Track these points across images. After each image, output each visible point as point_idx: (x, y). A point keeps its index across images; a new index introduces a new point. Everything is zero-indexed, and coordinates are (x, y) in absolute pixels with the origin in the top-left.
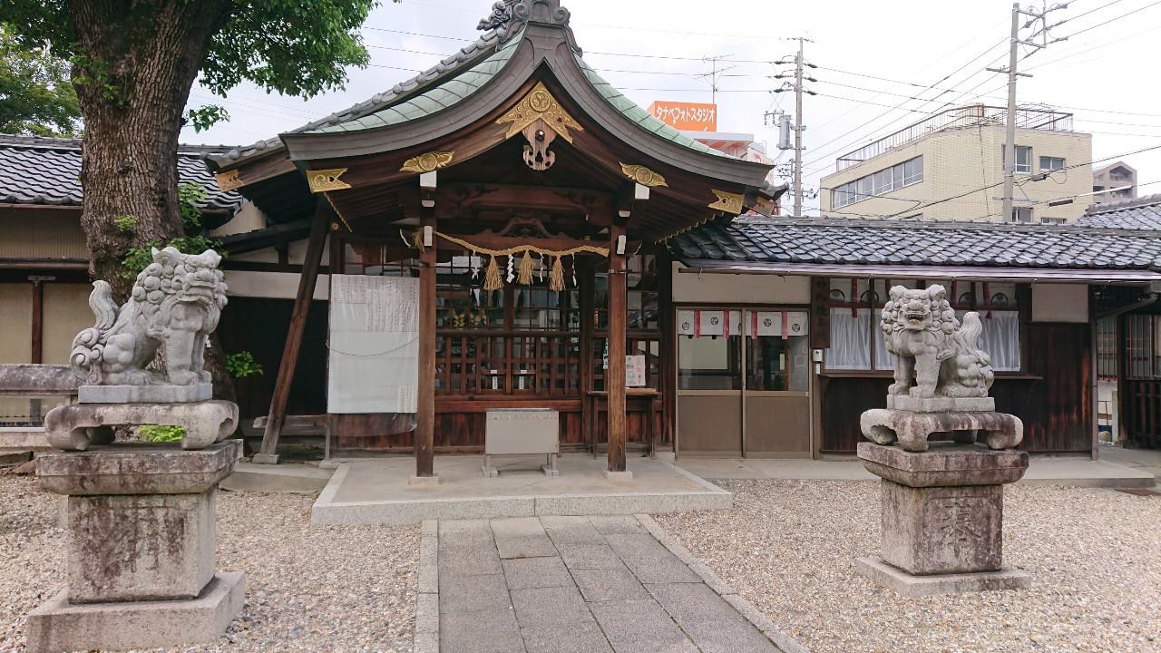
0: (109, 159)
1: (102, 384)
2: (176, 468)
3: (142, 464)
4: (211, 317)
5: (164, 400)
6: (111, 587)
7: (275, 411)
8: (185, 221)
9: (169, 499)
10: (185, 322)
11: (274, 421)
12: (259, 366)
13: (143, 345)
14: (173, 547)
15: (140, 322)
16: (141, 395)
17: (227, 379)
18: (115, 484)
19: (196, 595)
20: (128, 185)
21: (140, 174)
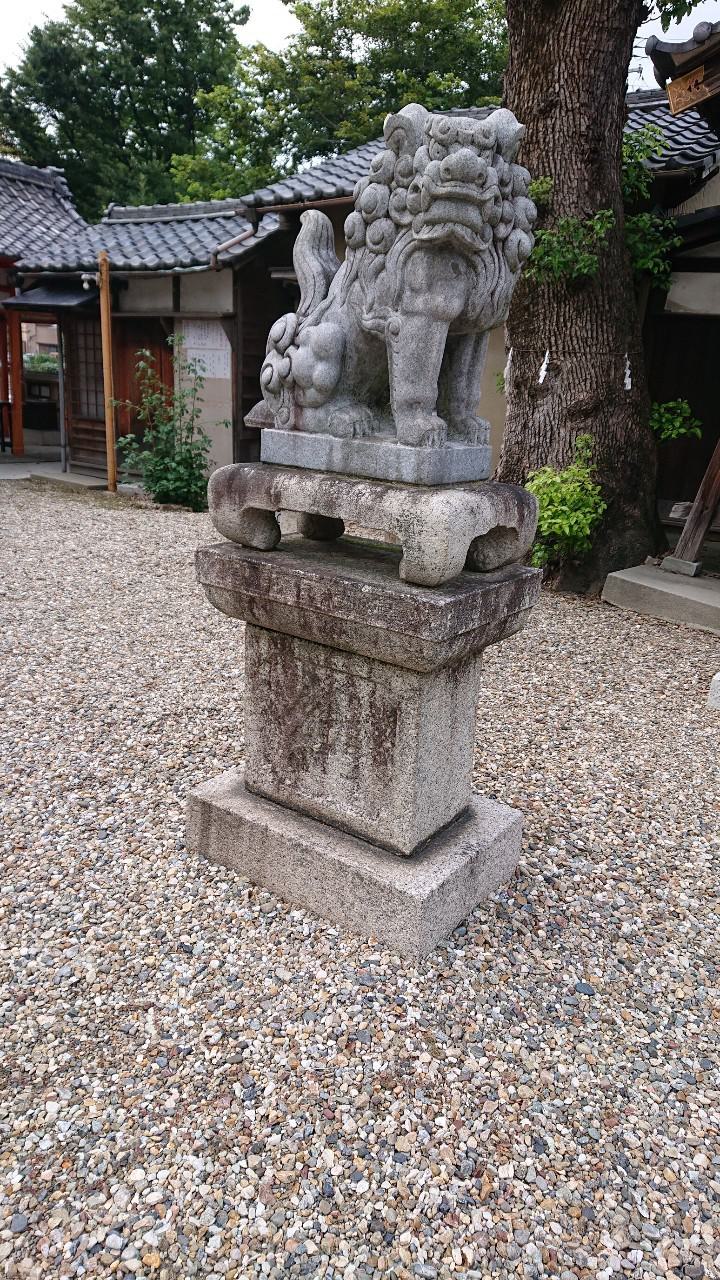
0: (529, 93)
1: (295, 428)
2: (378, 617)
3: (328, 597)
4: (484, 286)
5: (379, 474)
6: (295, 786)
7: (704, 497)
8: (628, 190)
9: (378, 669)
10: (428, 296)
11: (702, 512)
12: (697, 423)
13: (358, 350)
14: (379, 753)
15: (354, 298)
16: (346, 459)
17: (648, 440)
18: (293, 622)
19: (407, 852)
20: (550, 130)
21: (567, 111)
